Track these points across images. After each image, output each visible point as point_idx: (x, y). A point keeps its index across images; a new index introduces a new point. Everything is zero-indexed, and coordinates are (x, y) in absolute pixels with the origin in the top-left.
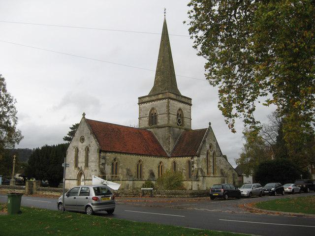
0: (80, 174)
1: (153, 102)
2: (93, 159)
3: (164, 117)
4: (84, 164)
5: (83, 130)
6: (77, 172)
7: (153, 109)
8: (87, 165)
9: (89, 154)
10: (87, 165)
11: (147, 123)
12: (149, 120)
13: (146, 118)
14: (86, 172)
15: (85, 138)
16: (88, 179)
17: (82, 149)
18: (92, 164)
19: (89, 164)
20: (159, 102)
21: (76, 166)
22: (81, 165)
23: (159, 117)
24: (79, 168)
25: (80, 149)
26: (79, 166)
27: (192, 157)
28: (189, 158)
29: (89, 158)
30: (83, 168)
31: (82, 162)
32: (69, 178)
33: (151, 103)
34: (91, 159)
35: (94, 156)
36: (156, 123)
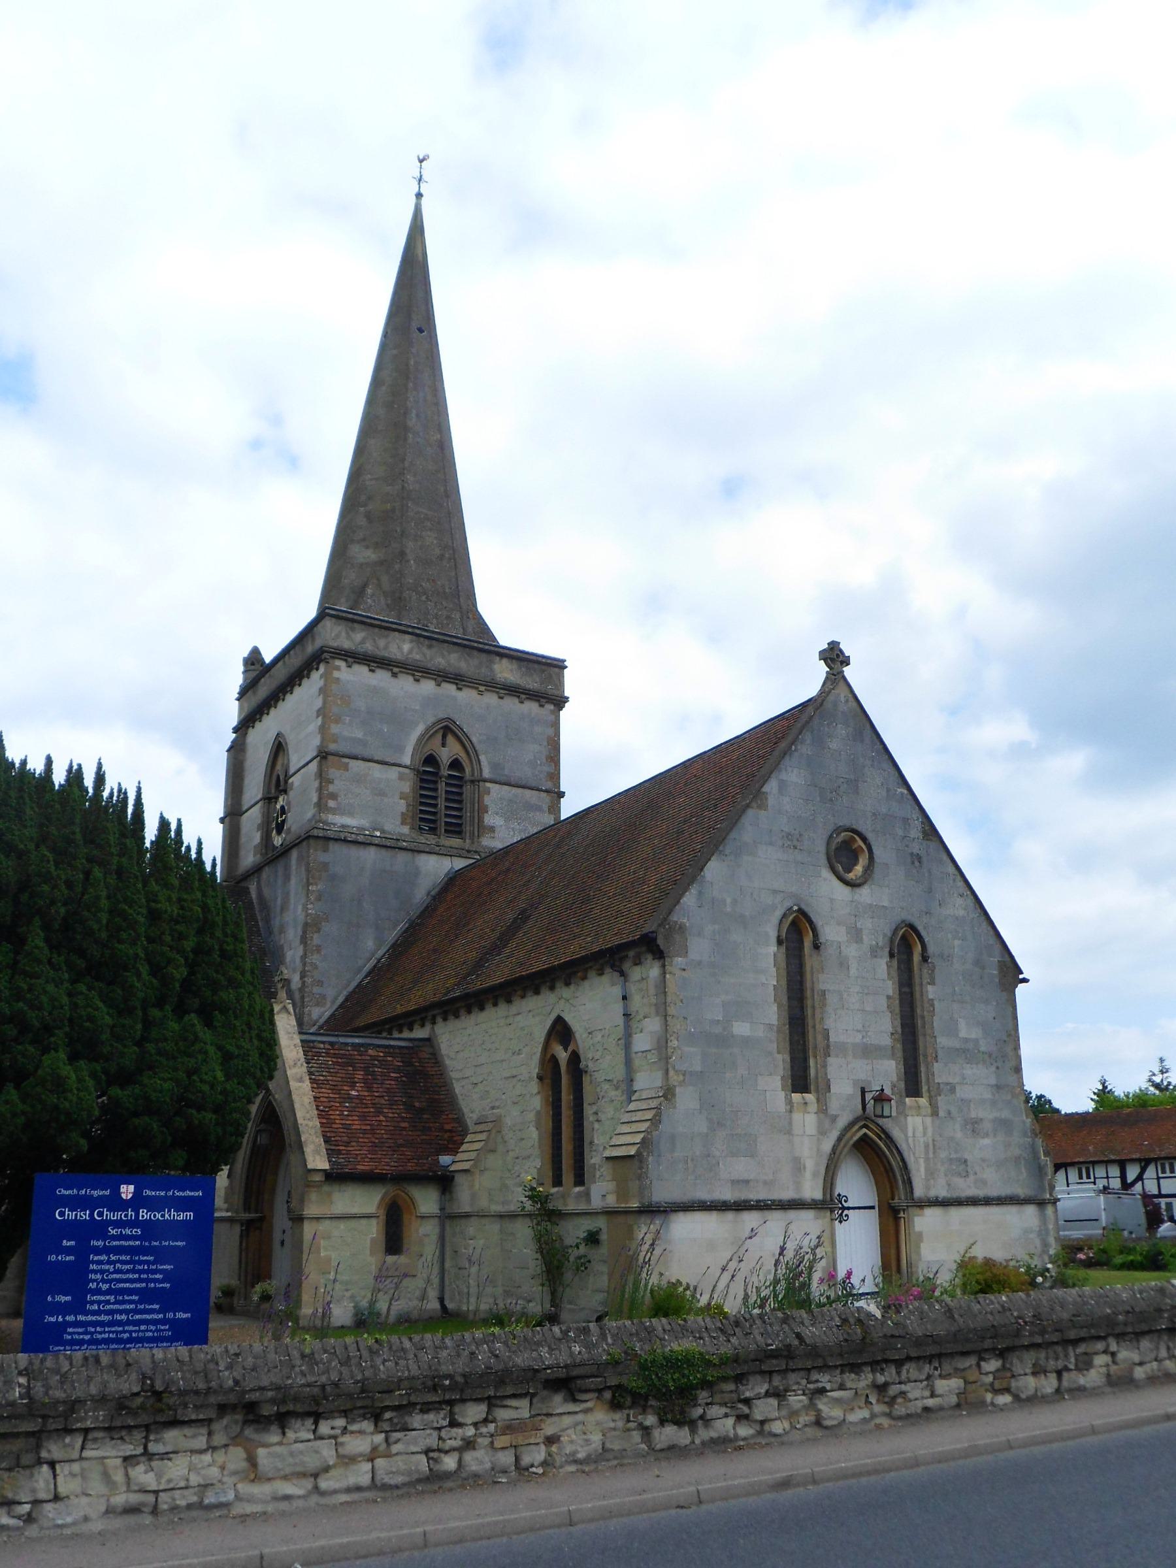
1: (450, 689)
2: (966, 1031)
3: (530, 807)
7: (447, 729)
11: (402, 806)
13: (393, 773)
17: (856, 935)
18: (970, 1071)
19: (941, 1072)
20: (491, 699)
23: (495, 795)
25: (831, 933)
31: (867, 1051)
32: (727, 1194)
34: (953, 1031)
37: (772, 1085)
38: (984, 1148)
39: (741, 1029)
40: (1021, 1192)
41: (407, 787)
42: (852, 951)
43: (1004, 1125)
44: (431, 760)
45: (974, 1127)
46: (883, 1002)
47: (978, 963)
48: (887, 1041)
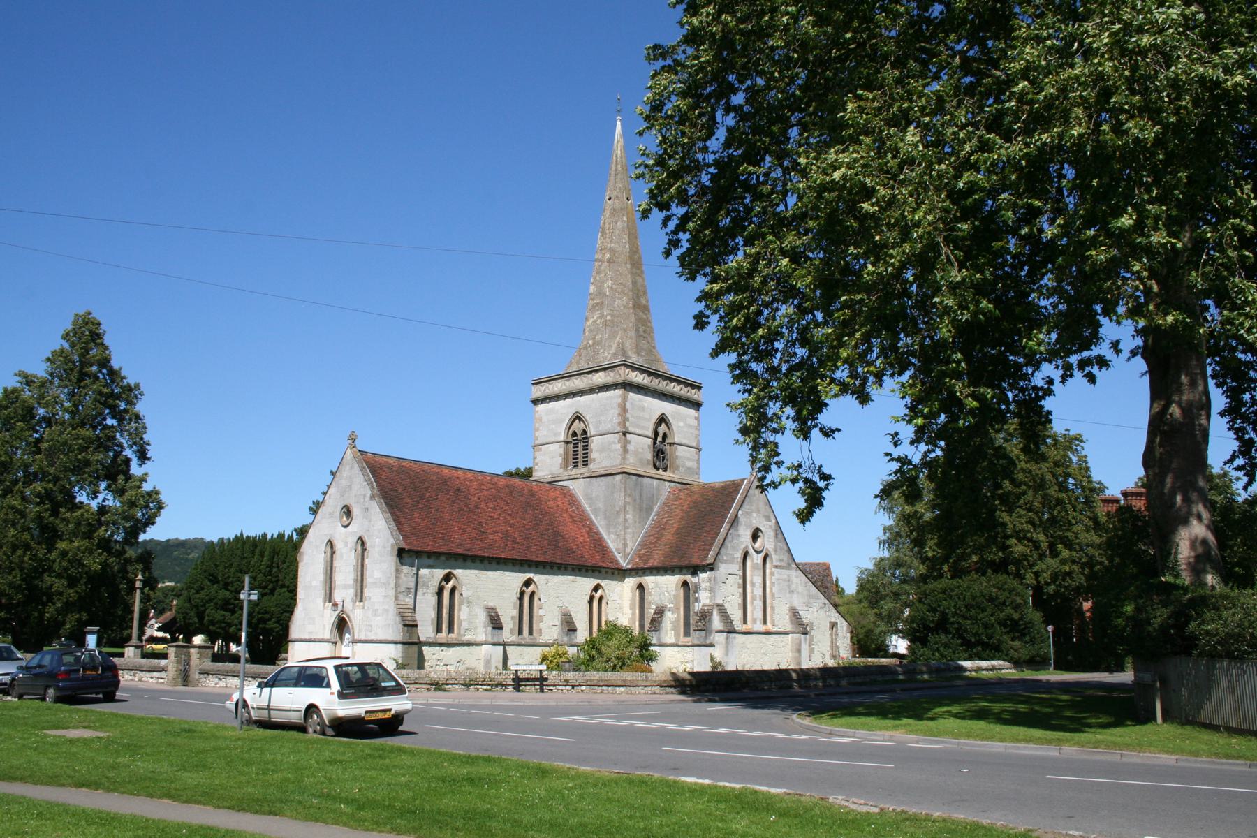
0: (342, 625)
2: (377, 574)
4: (351, 592)
5: (350, 487)
6: (330, 617)
7: (578, 417)
8: (360, 596)
9: (366, 561)
10: (360, 596)
11: (560, 460)
12: (566, 453)
14: (357, 617)
15: (356, 512)
16: (363, 638)
18: (377, 591)
19: (367, 593)
21: (329, 597)
22: (343, 594)
23: (595, 443)
24: (335, 605)
25: (339, 546)
26: (337, 596)
27: (695, 570)
28: (688, 578)
29: (367, 573)
30: (348, 606)
32: (307, 637)
33: (569, 401)
35: (382, 563)
36: (585, 463)
37: (320, 600)
38: (379, 621)
39: (314, 583)
40: (390, 638)
41: (562, 451)
42: (344, 551)
43: (386, 611)
44: (575, 434)
45: (375, 612)
46: (352, 568)
47: (384, 547)
48: (351, 582)
